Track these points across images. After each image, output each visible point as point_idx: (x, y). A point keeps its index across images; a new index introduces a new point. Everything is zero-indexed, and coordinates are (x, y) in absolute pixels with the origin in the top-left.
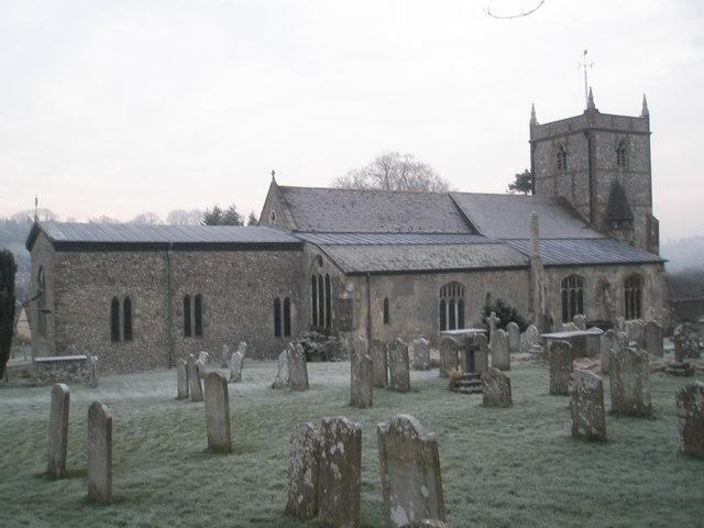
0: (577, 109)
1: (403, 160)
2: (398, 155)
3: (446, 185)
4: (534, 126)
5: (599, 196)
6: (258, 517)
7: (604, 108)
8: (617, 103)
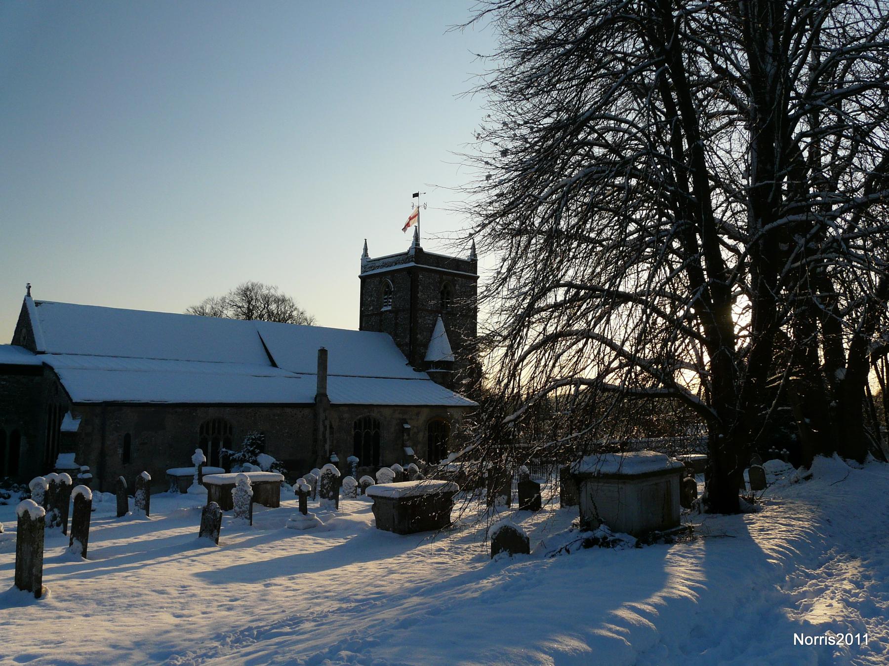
0: (402, 245)
4: (368, 264)
6: (72, 605)
7: (427, 246)
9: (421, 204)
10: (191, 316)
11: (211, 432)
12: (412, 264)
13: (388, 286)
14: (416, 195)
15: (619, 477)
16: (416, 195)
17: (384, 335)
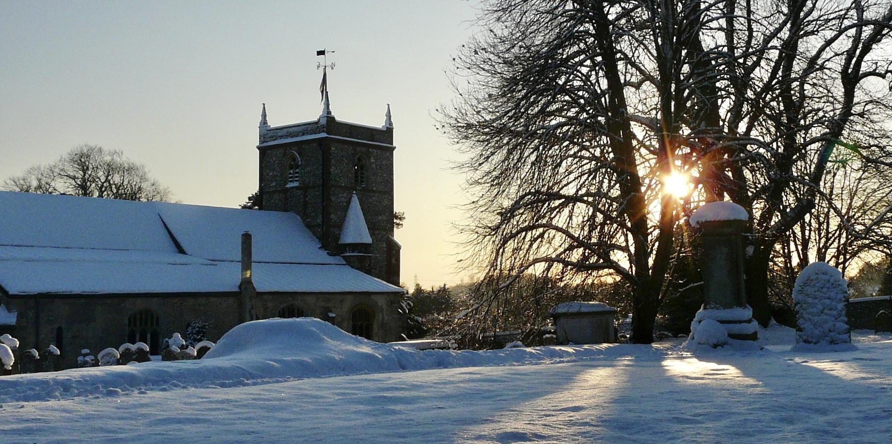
0: (312, 113)
1: (108, 158)
2: (100, 150)
3: (166, 192)
5: (332, 216)
7: (342, 115)
8: (356, 110)
9: (329, 63)
10: (12, 193)
11: (138, 323)
12: (324, 135)
13: (294, 159)
14: (321, 53)
15: (579, 314)
16: (321, 53)
17: (291, 214)
